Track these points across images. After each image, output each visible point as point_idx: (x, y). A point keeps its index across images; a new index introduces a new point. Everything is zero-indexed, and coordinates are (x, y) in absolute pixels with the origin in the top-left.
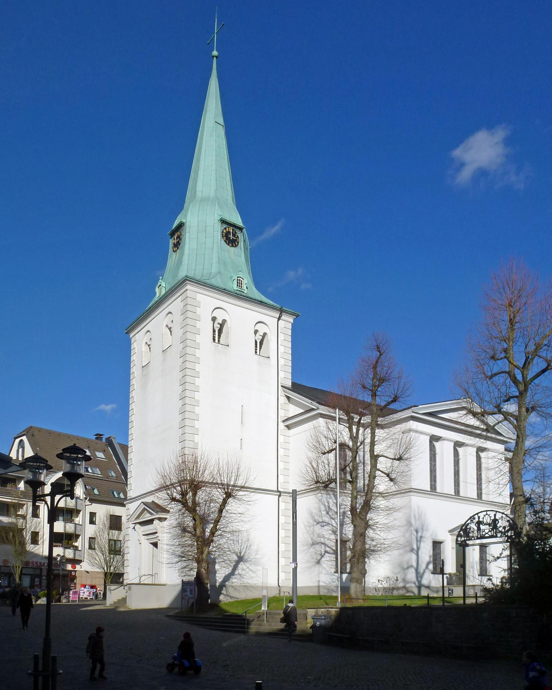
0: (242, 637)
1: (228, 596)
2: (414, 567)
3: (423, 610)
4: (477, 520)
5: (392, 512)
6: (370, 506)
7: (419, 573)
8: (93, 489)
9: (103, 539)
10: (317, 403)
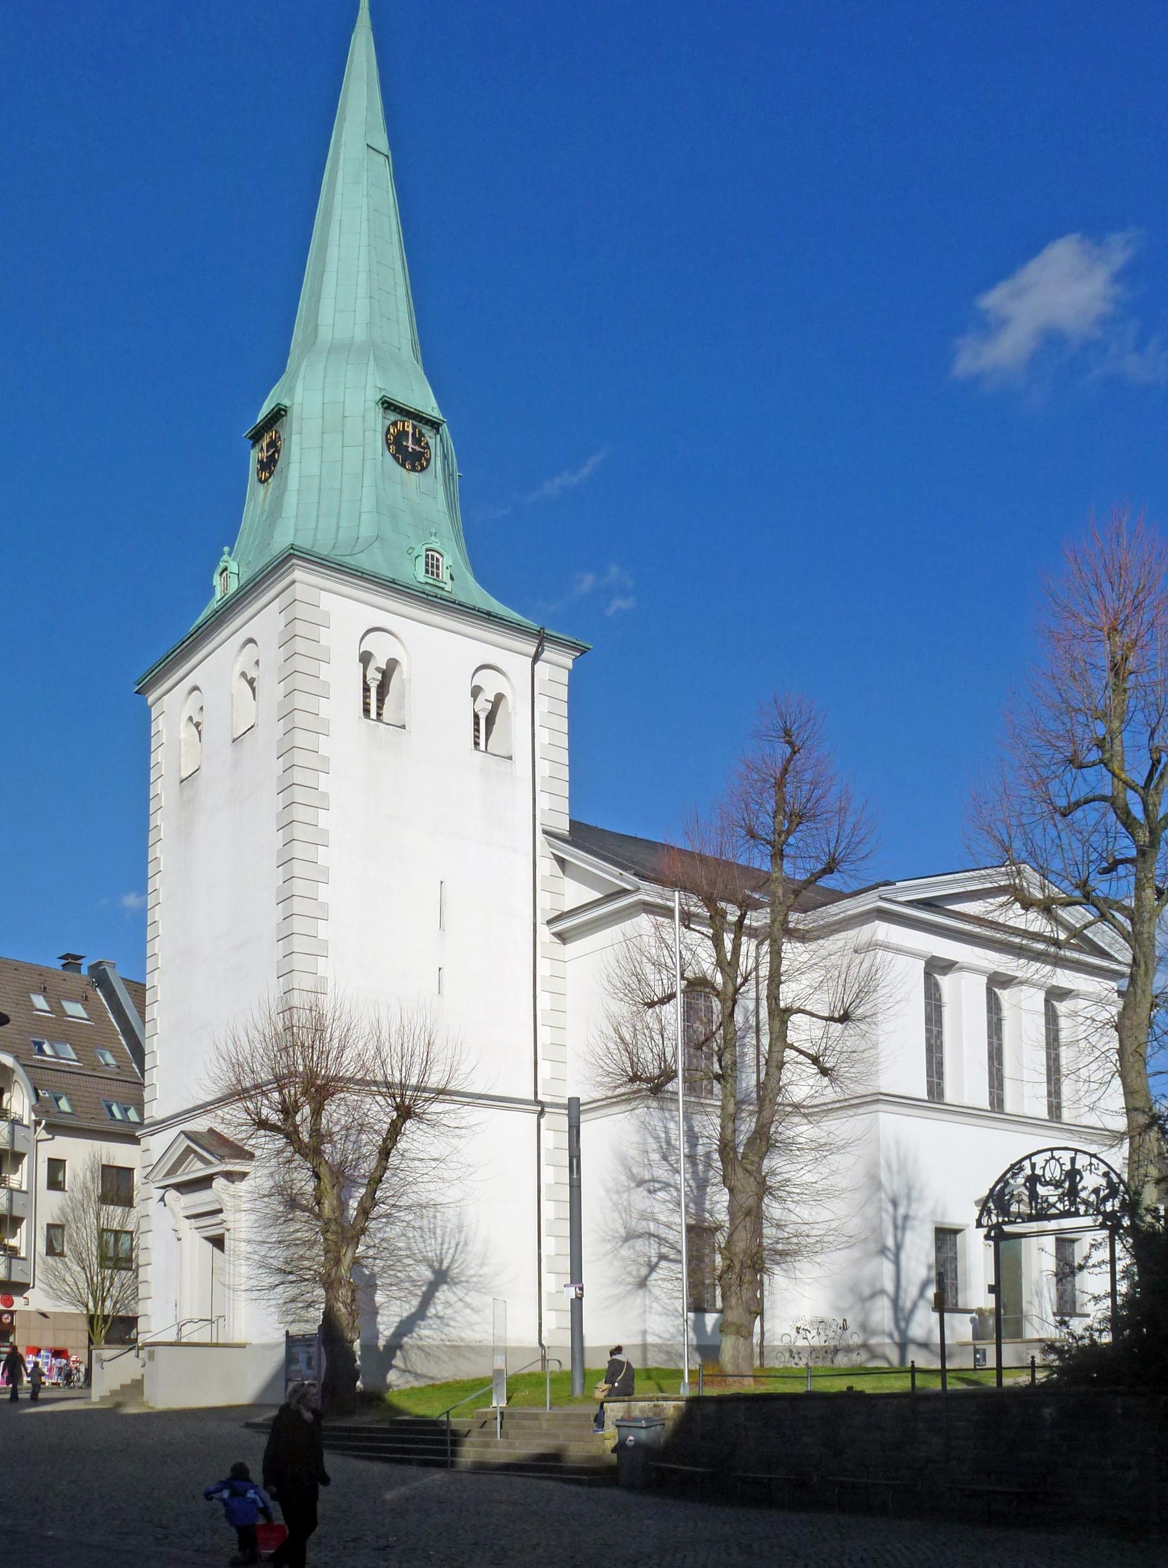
0: (437, 1476)
1: (409, 1372)
2: (888, 1295)
3: (895, 1402)
4: (1028, 1171)
5: (825, 1153)
6: (769, 1139)
7: (903, 1309)
8: (57, 1100)
9: (83, 1229)
10: (635, 874)
